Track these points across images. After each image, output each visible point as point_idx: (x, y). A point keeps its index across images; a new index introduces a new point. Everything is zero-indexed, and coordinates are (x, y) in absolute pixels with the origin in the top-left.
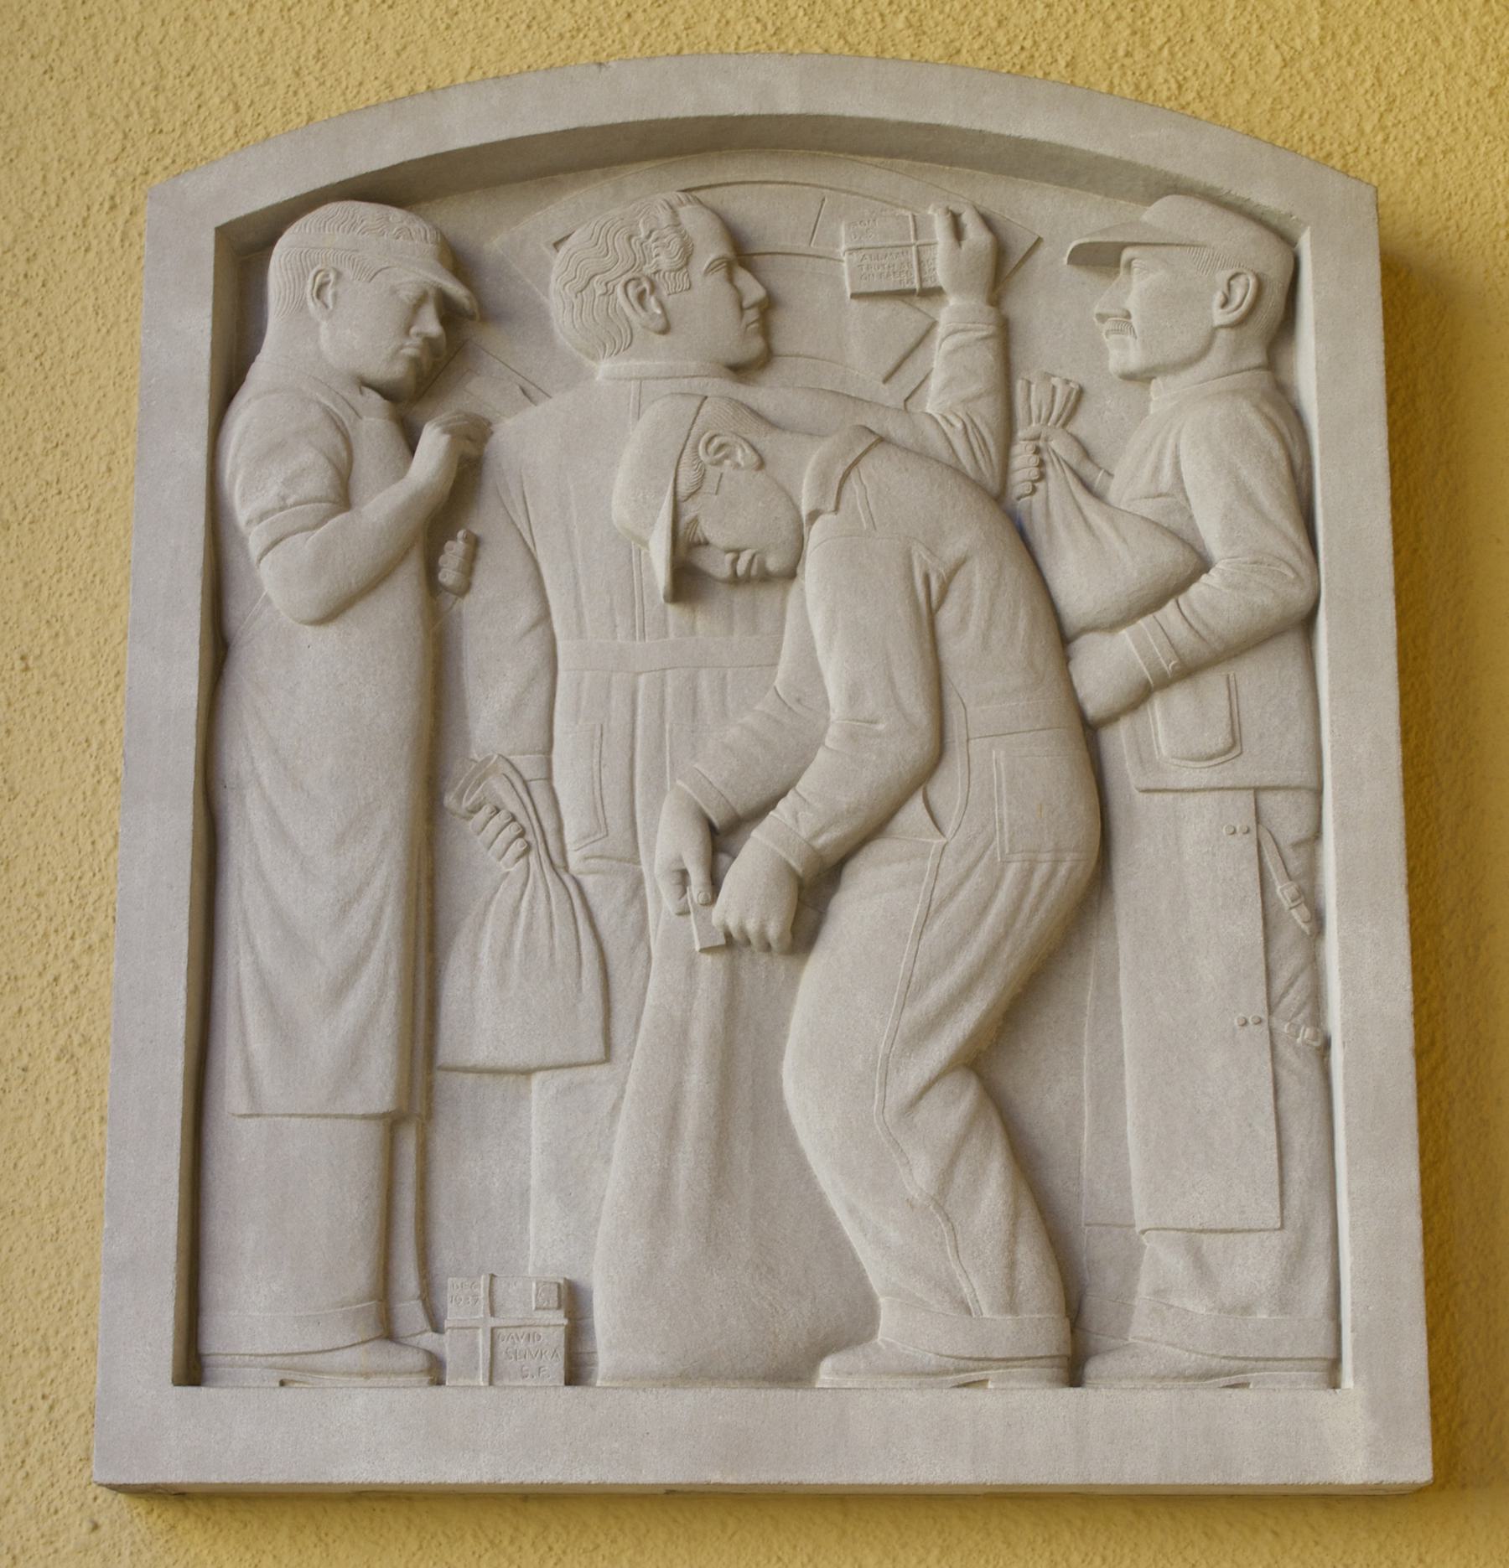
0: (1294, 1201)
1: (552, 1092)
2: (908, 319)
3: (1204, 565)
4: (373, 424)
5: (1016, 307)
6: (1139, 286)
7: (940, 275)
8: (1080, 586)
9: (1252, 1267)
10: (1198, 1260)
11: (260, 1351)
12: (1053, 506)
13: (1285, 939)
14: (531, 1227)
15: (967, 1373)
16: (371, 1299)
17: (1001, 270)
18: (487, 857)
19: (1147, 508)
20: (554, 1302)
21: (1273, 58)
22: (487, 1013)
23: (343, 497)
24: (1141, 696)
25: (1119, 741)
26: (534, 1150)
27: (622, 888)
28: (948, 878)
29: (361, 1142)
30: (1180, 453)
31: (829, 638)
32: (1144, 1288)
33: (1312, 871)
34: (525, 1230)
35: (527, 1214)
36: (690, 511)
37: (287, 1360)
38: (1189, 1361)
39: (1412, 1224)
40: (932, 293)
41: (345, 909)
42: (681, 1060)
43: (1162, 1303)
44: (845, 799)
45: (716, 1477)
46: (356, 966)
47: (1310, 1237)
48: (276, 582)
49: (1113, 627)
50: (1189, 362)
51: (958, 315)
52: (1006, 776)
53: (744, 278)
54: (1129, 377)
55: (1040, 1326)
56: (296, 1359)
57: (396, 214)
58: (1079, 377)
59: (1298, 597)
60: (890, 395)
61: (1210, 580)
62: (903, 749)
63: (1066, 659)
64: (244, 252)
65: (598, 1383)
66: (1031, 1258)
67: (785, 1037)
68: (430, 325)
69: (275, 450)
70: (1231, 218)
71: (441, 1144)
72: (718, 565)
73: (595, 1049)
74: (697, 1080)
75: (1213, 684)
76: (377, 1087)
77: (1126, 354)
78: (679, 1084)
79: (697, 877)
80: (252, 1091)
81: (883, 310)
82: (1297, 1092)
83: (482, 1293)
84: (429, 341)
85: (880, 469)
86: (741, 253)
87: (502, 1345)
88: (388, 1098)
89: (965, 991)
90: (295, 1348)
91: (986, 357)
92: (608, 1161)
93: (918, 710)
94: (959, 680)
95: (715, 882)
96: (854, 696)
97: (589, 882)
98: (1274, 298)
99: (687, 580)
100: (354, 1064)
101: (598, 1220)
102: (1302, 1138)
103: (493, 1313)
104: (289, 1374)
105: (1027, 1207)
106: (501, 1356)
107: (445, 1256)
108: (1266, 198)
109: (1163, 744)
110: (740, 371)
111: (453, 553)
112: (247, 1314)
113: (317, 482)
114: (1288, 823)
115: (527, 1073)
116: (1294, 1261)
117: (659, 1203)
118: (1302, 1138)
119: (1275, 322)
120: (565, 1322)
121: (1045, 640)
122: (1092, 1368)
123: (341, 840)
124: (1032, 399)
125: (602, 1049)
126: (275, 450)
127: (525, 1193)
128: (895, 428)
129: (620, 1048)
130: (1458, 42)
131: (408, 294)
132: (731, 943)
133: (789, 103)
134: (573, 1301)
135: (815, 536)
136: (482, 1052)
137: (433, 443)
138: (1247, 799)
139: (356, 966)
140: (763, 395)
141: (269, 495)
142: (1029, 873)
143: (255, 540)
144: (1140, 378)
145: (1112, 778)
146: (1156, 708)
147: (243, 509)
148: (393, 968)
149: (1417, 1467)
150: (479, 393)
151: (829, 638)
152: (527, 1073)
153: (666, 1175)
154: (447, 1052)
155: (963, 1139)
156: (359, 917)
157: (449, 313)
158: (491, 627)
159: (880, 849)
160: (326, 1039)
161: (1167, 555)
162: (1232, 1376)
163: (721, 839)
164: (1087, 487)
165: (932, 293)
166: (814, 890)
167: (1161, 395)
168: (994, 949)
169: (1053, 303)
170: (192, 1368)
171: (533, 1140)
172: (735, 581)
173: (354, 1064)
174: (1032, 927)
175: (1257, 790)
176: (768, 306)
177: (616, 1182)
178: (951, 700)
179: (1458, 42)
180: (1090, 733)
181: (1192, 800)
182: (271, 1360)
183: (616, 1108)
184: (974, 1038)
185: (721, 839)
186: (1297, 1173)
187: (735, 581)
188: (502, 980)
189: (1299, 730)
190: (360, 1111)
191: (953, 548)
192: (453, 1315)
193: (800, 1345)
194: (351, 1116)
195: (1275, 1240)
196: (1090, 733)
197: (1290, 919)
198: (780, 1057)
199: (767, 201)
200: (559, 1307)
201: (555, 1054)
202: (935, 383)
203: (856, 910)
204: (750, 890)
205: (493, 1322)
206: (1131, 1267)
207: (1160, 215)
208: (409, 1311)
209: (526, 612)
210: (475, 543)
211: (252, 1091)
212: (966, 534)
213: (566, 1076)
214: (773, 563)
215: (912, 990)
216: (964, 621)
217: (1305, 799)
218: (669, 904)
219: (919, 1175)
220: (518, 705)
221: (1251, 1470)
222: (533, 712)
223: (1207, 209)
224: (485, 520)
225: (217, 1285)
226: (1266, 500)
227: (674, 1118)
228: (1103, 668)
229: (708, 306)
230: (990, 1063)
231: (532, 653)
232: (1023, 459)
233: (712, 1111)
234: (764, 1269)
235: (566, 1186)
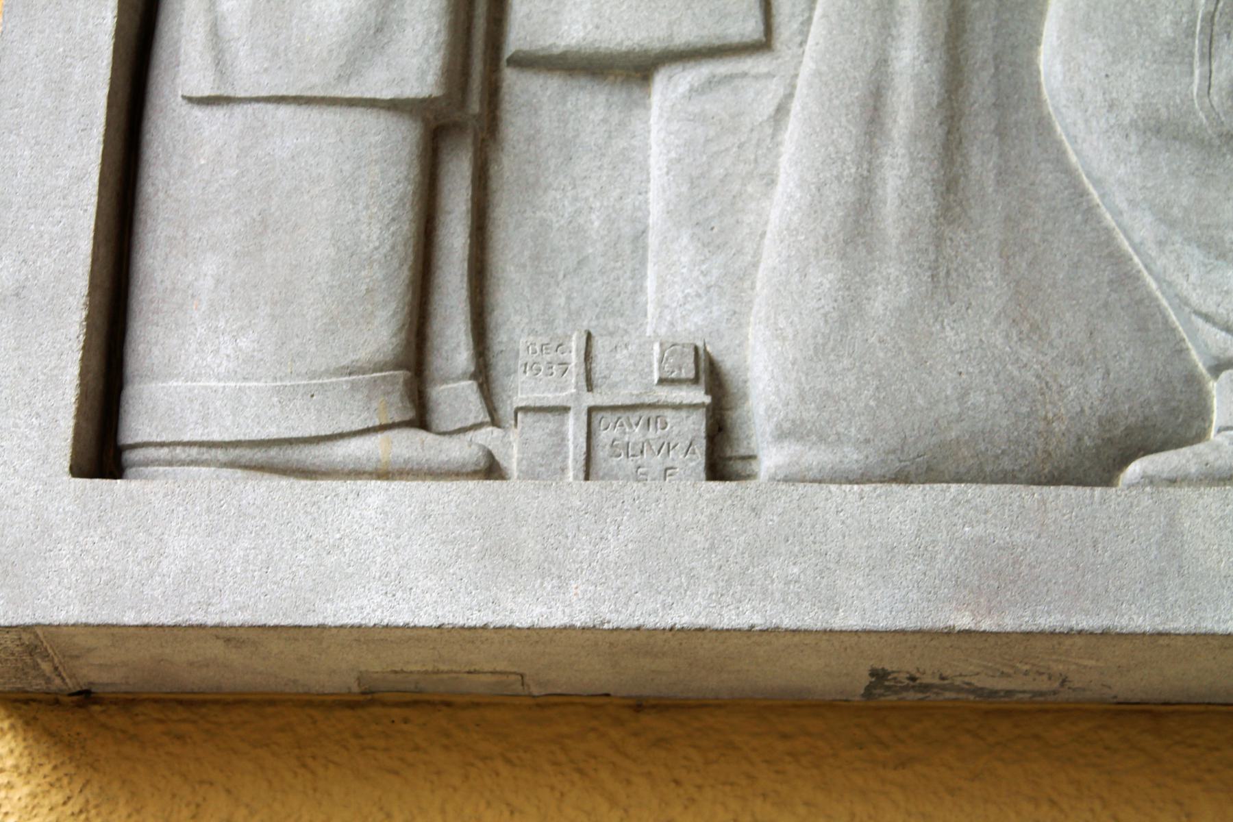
1: (683, 88)
11: (216, 437)
14: (651, 284)
16: (397, 366)
20: (688, 372)
26: (654, 173)
29: (381, 157)
34: (639, 289)
35: (643, 262)
37: (259, 455)
42: (886, 30)
45: (964, 621)
56: (273, 452)
67: (1042, 14)
71: (508, 167)
73: (750, 28)
78: (882, 63)
80: (220, 63)
83: (574, 358)
87: (604, 436)
88: (431, 78)
90: (273, 432)
92: (772, 182)
100: (379, 30)
101: (755, 265)
103: (590, 386)
106: (601, 453)
107: (515, 328)
112: (190, 378)
115: (634, 70)
117: (857, 227)
120: (707, 400)
125: (761, 27)
127: (640, 236)
129: (786, 28)
152: (634, 70)
153: (866, 185)
170: (102, 449)
171: (652, 161)
173: (379, 30)
182: (234, 453)
183: (781, 110)
190: (387, 94)
192: (522, 388)
193: (1087, 441)
194: (372, 104)
198: (1035, 41)
200: (696, 381)
201: (687, 34)
205: (591, 400)
208: (455, 396)
211: (220, 63)
213: (706, 69)
225: (150, 342)
227: (876, 109)
233: (935, 100)
234: (1025, 327)
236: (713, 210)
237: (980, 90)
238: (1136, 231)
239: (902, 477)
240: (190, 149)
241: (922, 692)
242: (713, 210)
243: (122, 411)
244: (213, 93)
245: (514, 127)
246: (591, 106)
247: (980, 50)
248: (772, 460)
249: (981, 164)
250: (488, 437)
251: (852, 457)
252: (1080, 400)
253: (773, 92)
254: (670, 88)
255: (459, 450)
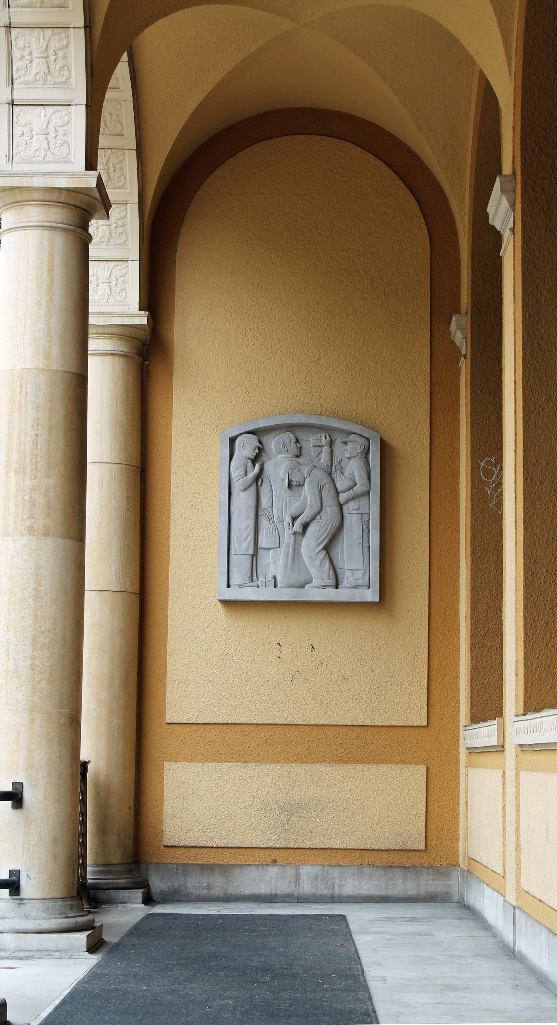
0: (365, 566)
2: (319, 449)
3: (356, 484)
4: (250, 464)
5: (334, 448)
6: (349, 447)
7: (323, 443)
8: (340, 487)
9: (359, 575)
10: (352, 573)
12: (337, 476)
13: (365, 533)
15: (324, 587)
17: (331, 444)
18: (264, 523)
19: (349, 476)
21: (370, 410)
22: (263, 542)
23: (246, 475)
24: (347, 502)
25: (345, 508)
27: (281, 525)
28: (322, 525)
30: (354, 468)
31: (308, 494)
32: (346, 578)
33: (369, 524)
36: (290, 477)
38: (351, 586)
39: (378, 569)
40: (322, 446)
41: (247, 528)
43: (348, 579)
44: (310, 515)
46: (248, 536)
47: (366, 571)
48: (237, 486)
49: (344, 492)
50: (355, 457)
51: (326, 449)
52: (330, 511)
53: (298, 444)
54: (348, 458)
55: (332, 581)
57: (253, 436)
58: (341, 457)
59: (368, 489)
60: (317, 459)
61: (357, 486)
62: (316, 509)
63: (338, 496)
64: (232, 441)
65: (331, 892)
66: (332, 573)
68: (257, 451)
69: (238, 468)
70: (361, 437)
71: (258, 557)
72: (294, 484)
73: (278, 546)
74: (291, 550)
75: (357, 500)
76: (251, 551)
77: (347, 455)
79: (291, 524)
80: (236, 551)
81: (316, 448)
82: (366, 552)
84: (257, 453)
85: (315, 471)
86: (297, 441)
89: (324, 540)
91: (329, 455)
93: (319, 504)
94: (324, 499)
95: (293, 525)
96: (311, 501)
97: (277, 524)
98: (366, 448)
99: (290, 485)
102: (366, 558)
104: (241, 586)
105: (331, 566)
107: (259, 572)
108: (366, 435)
109: (350, 508)
110: (298, 456)
111: (260, 480)
112: (235, 579)
113: (243, 473)
114: (366, 518)
115: (269, 549)
116: (364, 574)
117: (286, 566)
118: (366, 558)
119: (366, 452)
121: (335, 494)
122: (339, 586)
123: (246, 519)
124: (335, 460)
126: (238, 468)
128: (317, 465)
130: (395, 408)
131: (254, 447)
132: (295, 533)
133: (304, 421)
134: (275, 578)
135: (306, 480)
136: (264, 546)
137: (257, 466)
138: (360, 515)
139: (248, 536)
140: (300, 460)
141: (237, 474)
142: (332, 525)
143: (235, 480)
144: (349, 458)
145: (344, 512)
146: (350, 503)
147: (233, 476)
148: (253, 535)
149: (377, 599)
150: (264, 458)
151: (308, 494)
152: (269, 549)
153: (287, 562)
154: (260, 545)
155: (323, 558)
156: (249, 529)
157: (259, 449)
158: (264, 491)
159: (314, 521)
160: (245, 545)
161: (351, 483)
162: (356, 587)
163: (294, 519)
164: (342, 473)
165: (322, 446)
166: (305, 526)
167: (352, 461)
168: (328, 534)
169: (338, 447)
170: (228, 586)
172: (296, 486)
174: (333, 531)
175: (362, 514)
176: (301, 448)
177: (280, 563)
178: (323, 502)
179: (395, 408)
180: (341, 506)
181: (353, 515)
184: (325, 545)
185: (294, 519)
186: (365, 562)
187: (296, 486)
188: (266, 537)
189: (368, 505)
191: (324, 482)
192: (260, 579)
195: (362, 571)
196: (341, 506)
197: (365, 530)
199: (301, 435)
201: (273, 547)
202: (323, 458)
203: (310, 530)
204: (298, 526)
206: (344, 574)
207: (352, 437)
208: (255, 578)
209: (269, 489)
210: (262, 480)
211: (236, 551)
212: (326, 480)
214: (301, 483)
215: (318, 539)
216: (325, 492)
217: (368, 515)
218: (287, 528)
219: (318, 563)
220: (268, 501)
221: (357, 599)
222: (270, 502)
223: (358, 436)
224: (264, 476)
226: (364, 476)
228: (343, 497)
229: (293, 448)
230: (327, 549)
231: (270, 494)
232: (334, 468)
235: (274, 564)
236: (275, 562)
237: (296, 552)
238: (308, 566)
239: (289, 587)
240: (233, 558)
241: (279, 518)
242: (275, 562)
243: (140, 425)
244: (383, 893)
245: (259, 554)
246: (265, 551)
247: (297, 549)
248: (279, 585)
249: (296, 559)
250: (257, 582)
251: (285, 585)
252: (303, 580)
253: (280, 552)
254: (271, 551)
255: (255, 584)
